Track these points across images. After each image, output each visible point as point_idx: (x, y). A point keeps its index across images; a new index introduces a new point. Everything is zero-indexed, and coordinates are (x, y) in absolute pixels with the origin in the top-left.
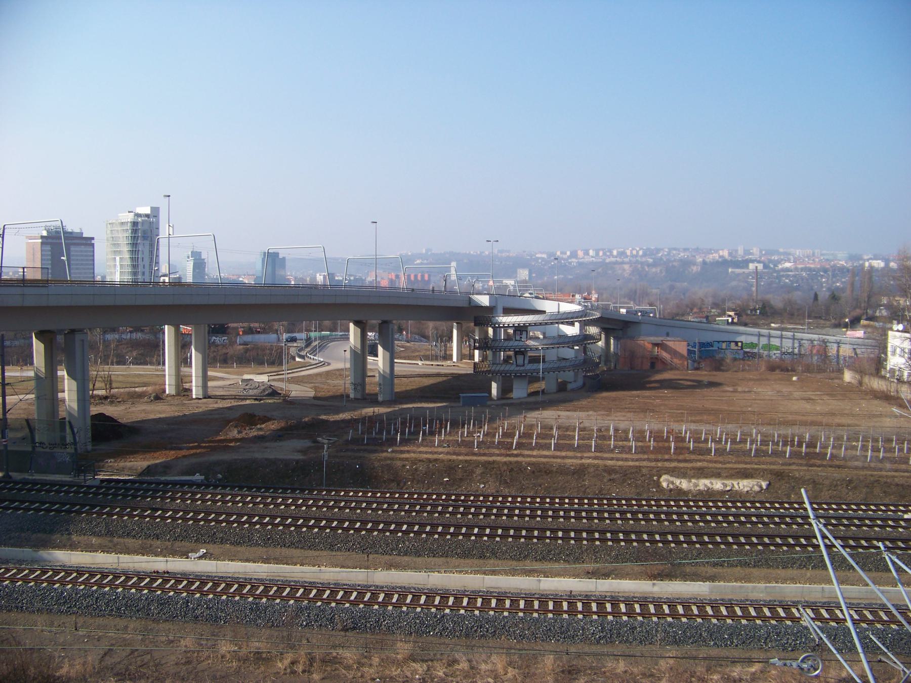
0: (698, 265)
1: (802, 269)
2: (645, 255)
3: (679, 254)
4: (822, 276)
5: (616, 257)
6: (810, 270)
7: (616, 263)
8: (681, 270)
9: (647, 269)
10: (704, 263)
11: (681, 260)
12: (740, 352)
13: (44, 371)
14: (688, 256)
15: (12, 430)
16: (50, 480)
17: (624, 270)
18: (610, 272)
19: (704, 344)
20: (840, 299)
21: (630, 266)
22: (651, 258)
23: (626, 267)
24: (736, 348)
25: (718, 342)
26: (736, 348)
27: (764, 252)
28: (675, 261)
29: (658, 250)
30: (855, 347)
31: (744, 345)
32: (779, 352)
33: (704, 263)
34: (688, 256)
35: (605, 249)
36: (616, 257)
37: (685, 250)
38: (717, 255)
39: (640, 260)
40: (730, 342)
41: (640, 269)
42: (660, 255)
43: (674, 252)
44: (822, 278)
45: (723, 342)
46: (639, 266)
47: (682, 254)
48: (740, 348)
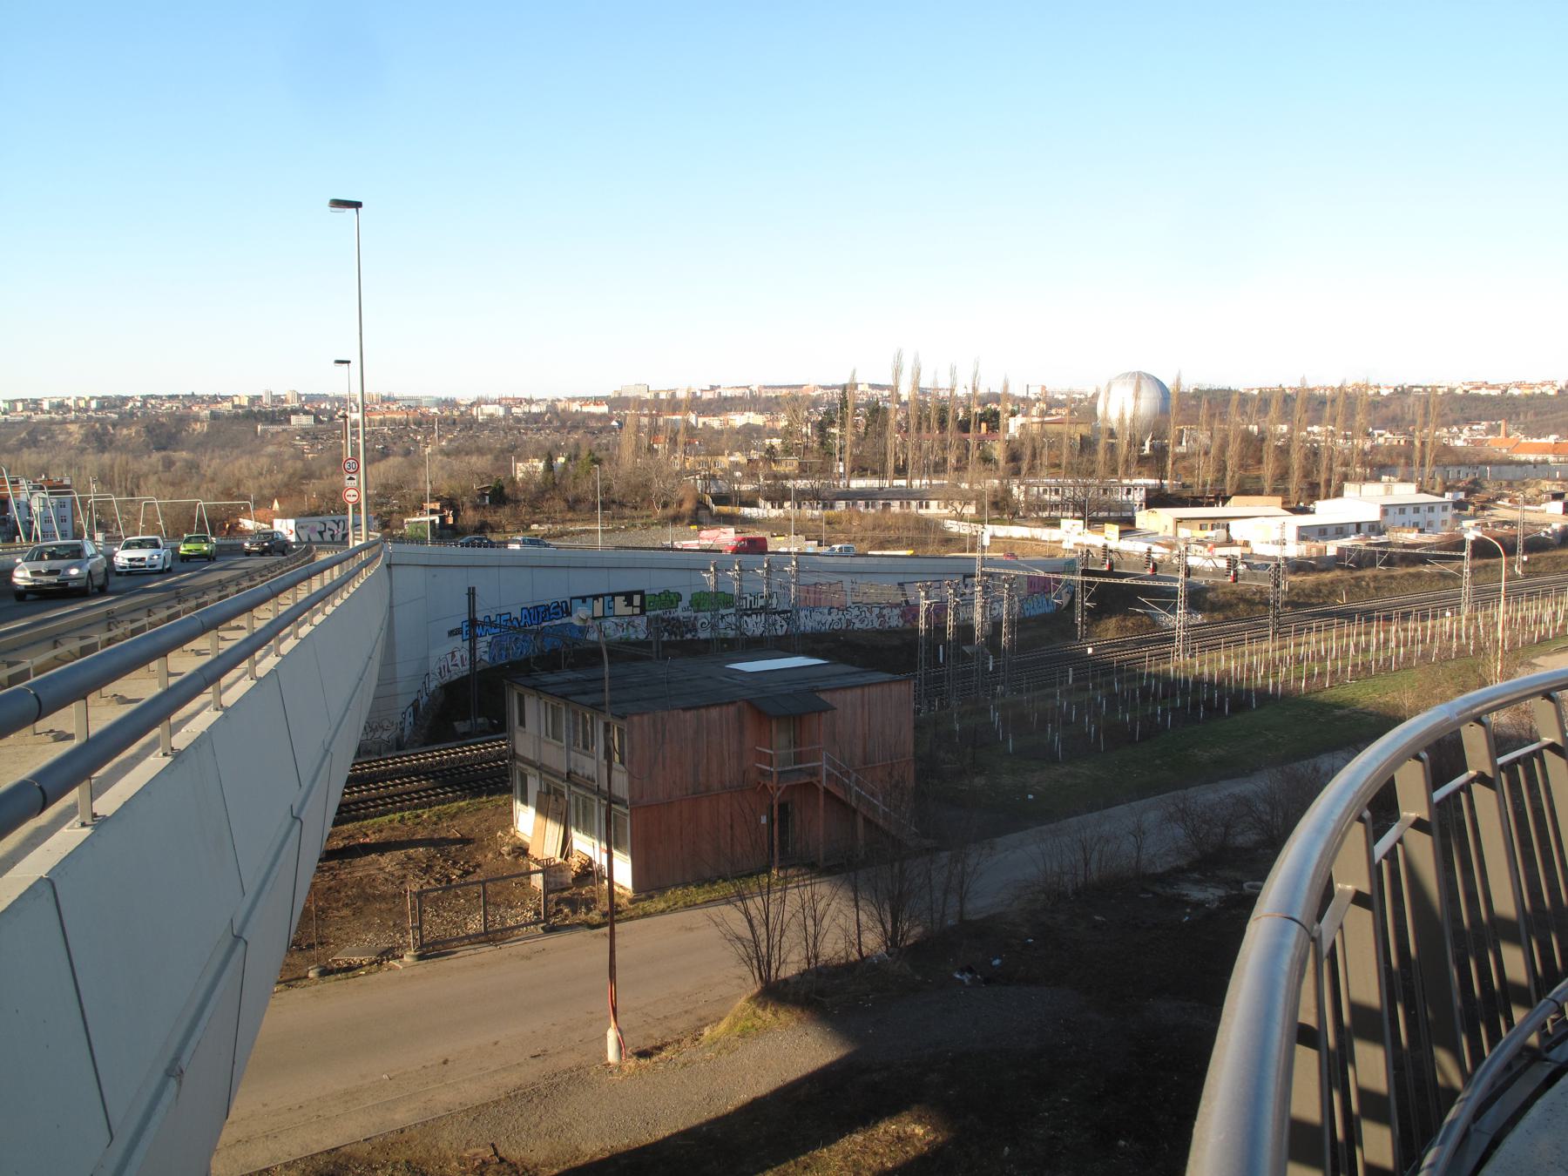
0: (202, 422)
1: (382, 423)
2: (101, 407)
3: (162, 405)
4: (416, 432)
5: (49, 412)
6: (394, 421)
7: (52, 422)
8: (174, 430)
9: (112, 431)
10: (215, 416)
11: (171, 415)
12: (637, 621)
13: (77, 789)
14: (177, 407)
15: (605, 935)
16: (1322, 856)
17: (70, 434)
18: (43, 438)
19: (547, 608)
20: (646, 485)
21: (81, 427)
22: (115, 413)
23: (73, 428)
24: (629, 611)
25: (584, 599)
26: (629, 611)
27: (303, 399)
28: (163, 416)
29: (125, 400)
30: (901, 579)
31: (647, 599)
32: (732, 610)
33: (215, 416)
34: (177, 407)
35: (26, 400)
36: (49, 412)
37: (172, 398)
38: (230, 404)
39: (93, 414)
40: (613, 595)
41: (100, 430)
42: (128, 407)
43: (153, 402)
44: (415, 435)
45: (596, 597)
46: (98, 425)
47: (167, 405)
48: (637, 611)
